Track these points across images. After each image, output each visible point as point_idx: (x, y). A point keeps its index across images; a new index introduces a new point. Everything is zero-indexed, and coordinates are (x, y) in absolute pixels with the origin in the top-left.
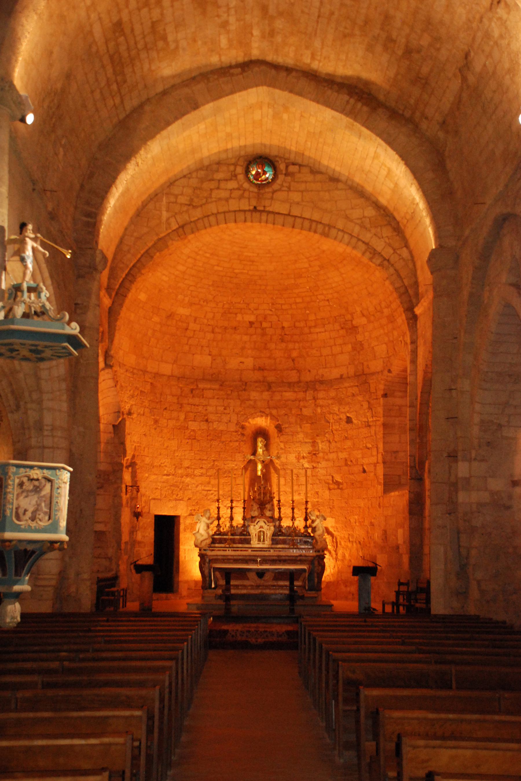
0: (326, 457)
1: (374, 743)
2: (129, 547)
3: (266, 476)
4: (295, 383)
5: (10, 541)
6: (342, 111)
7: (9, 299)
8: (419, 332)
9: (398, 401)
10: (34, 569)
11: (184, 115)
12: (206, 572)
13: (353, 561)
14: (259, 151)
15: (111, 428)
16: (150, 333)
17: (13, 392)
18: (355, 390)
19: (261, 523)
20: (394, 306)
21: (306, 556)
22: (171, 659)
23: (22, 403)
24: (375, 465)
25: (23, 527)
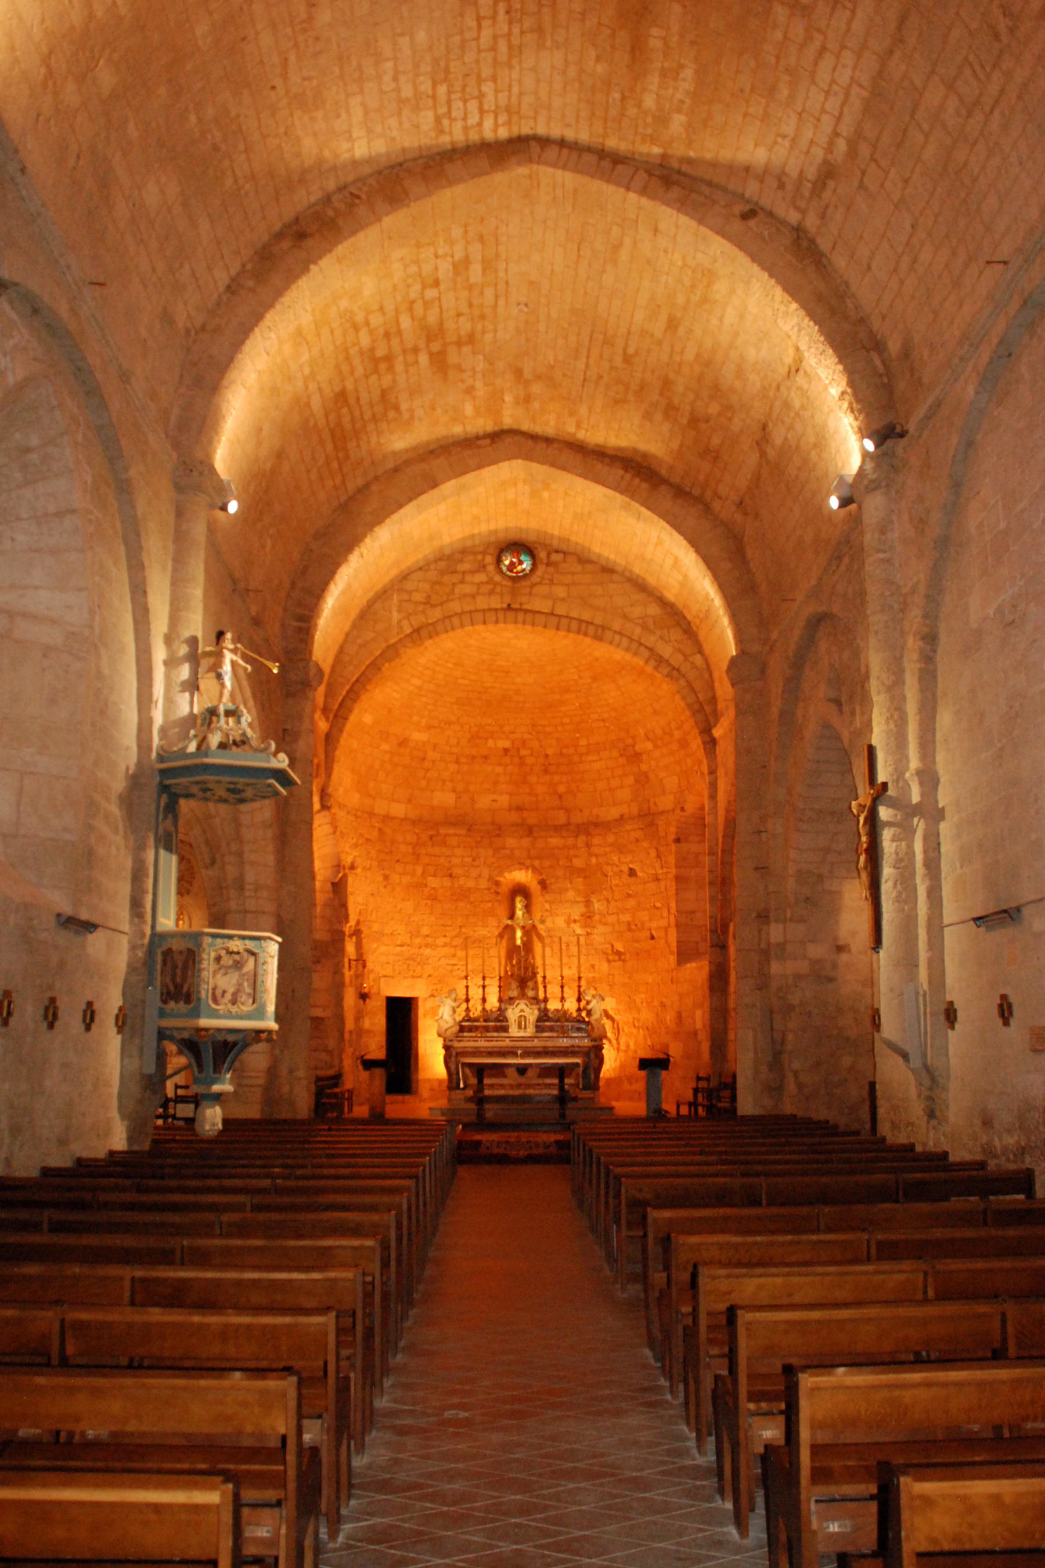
0: (604, 920)
1: (665, 1275)
2: (354, 1037)
3: (528, 946)
4: (562, 826)
5: (206, 1030)
6: (616, 488)
7: (202, 725)
8: (719, 759)
9: (695, 848)
10: (237, 1064)
11: (419, 494)
12: (453, 1067)
13: (639, 1052)
14: (513, 536)
15: (329, 887)
16: (377, 764)
17: (207, 842)
18: (639, 834)
19: (522, 1006)
20: (687, 727)
21: (579, 1047)
22: (410, 1177)
23: (218, 856)
24: (666, 929)
25: (221, 1012)
